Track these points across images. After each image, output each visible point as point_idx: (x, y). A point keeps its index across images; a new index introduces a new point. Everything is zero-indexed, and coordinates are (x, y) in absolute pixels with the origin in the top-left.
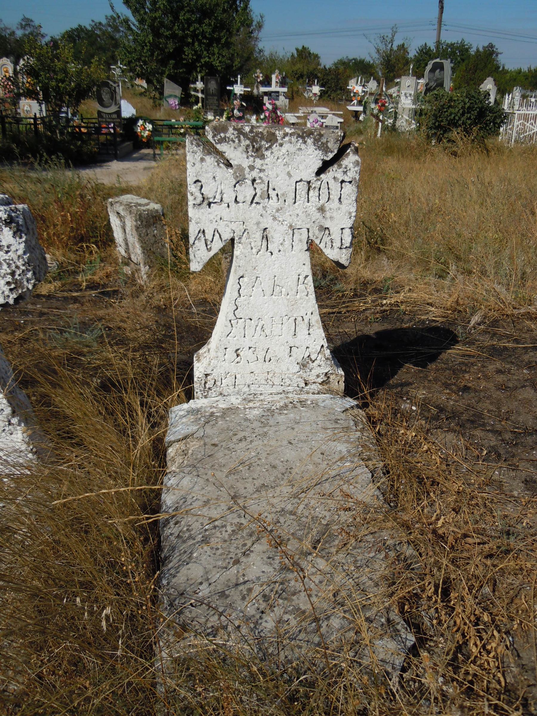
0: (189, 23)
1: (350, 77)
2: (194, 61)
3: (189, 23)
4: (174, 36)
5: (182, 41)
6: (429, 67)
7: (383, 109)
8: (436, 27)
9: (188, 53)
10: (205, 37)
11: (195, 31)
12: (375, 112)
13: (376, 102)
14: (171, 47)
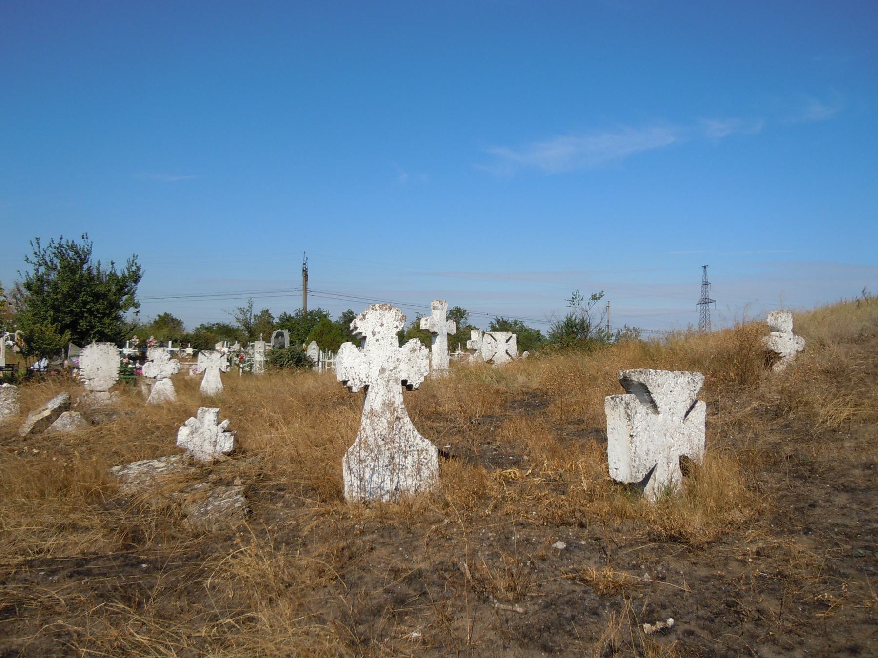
0: (85, 303)
1: (217, 342)
2: (88, 330)
3: (85, 303)
4: (71, 312)
5: (81, 315)
6: (274, 335)
7: (242, 360)
8: (302, 293)
9: (83, 324)
10: (99, 313)
11: (90, 308)
12: (237, 362)
13: (237, 356)
14: (68, 319)
